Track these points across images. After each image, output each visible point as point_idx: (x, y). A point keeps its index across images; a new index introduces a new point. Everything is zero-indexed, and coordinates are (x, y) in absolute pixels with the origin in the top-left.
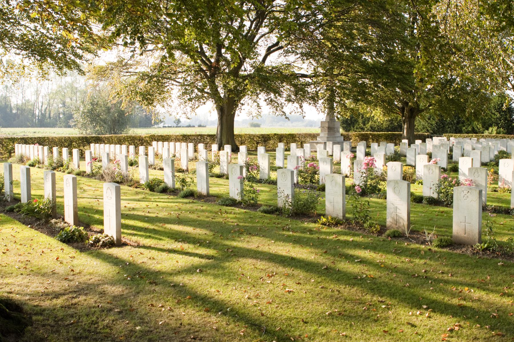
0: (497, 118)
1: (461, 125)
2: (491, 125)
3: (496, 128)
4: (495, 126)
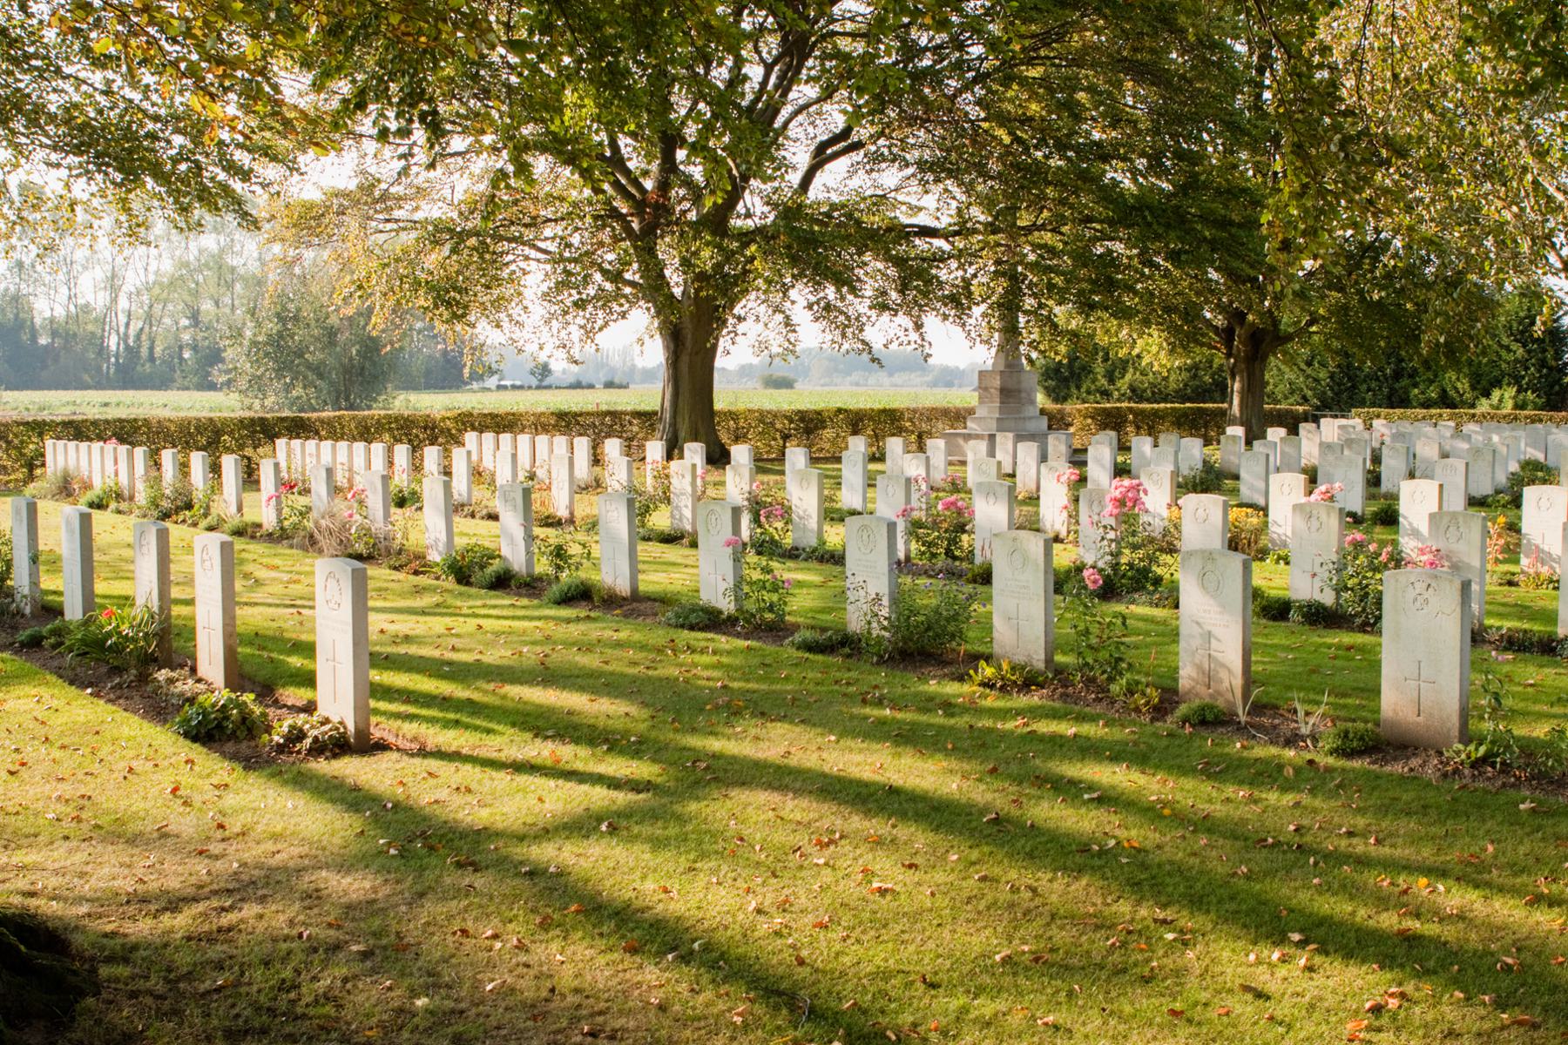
2: (1497, 383)
3: (1512, 391)
4: (1509, 384)
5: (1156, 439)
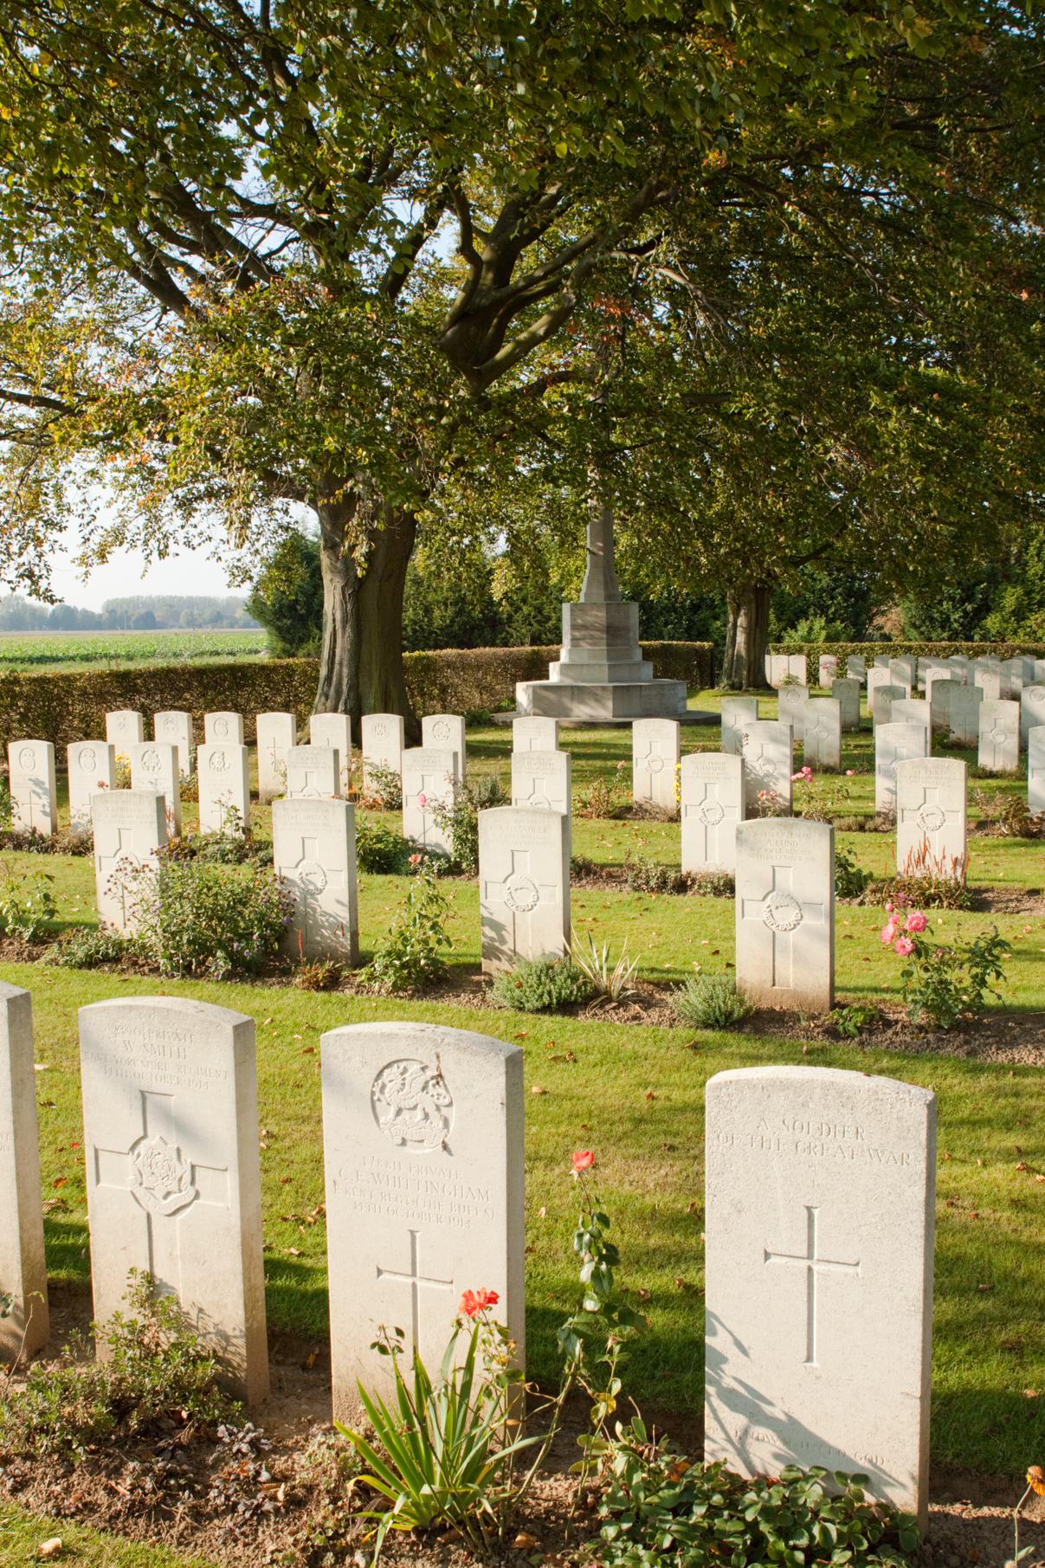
0: (822, 590)
1: (704, 614)
2: (802, 614)
3: (819, 622)
4: (815, 615)
5: (301, 723)
